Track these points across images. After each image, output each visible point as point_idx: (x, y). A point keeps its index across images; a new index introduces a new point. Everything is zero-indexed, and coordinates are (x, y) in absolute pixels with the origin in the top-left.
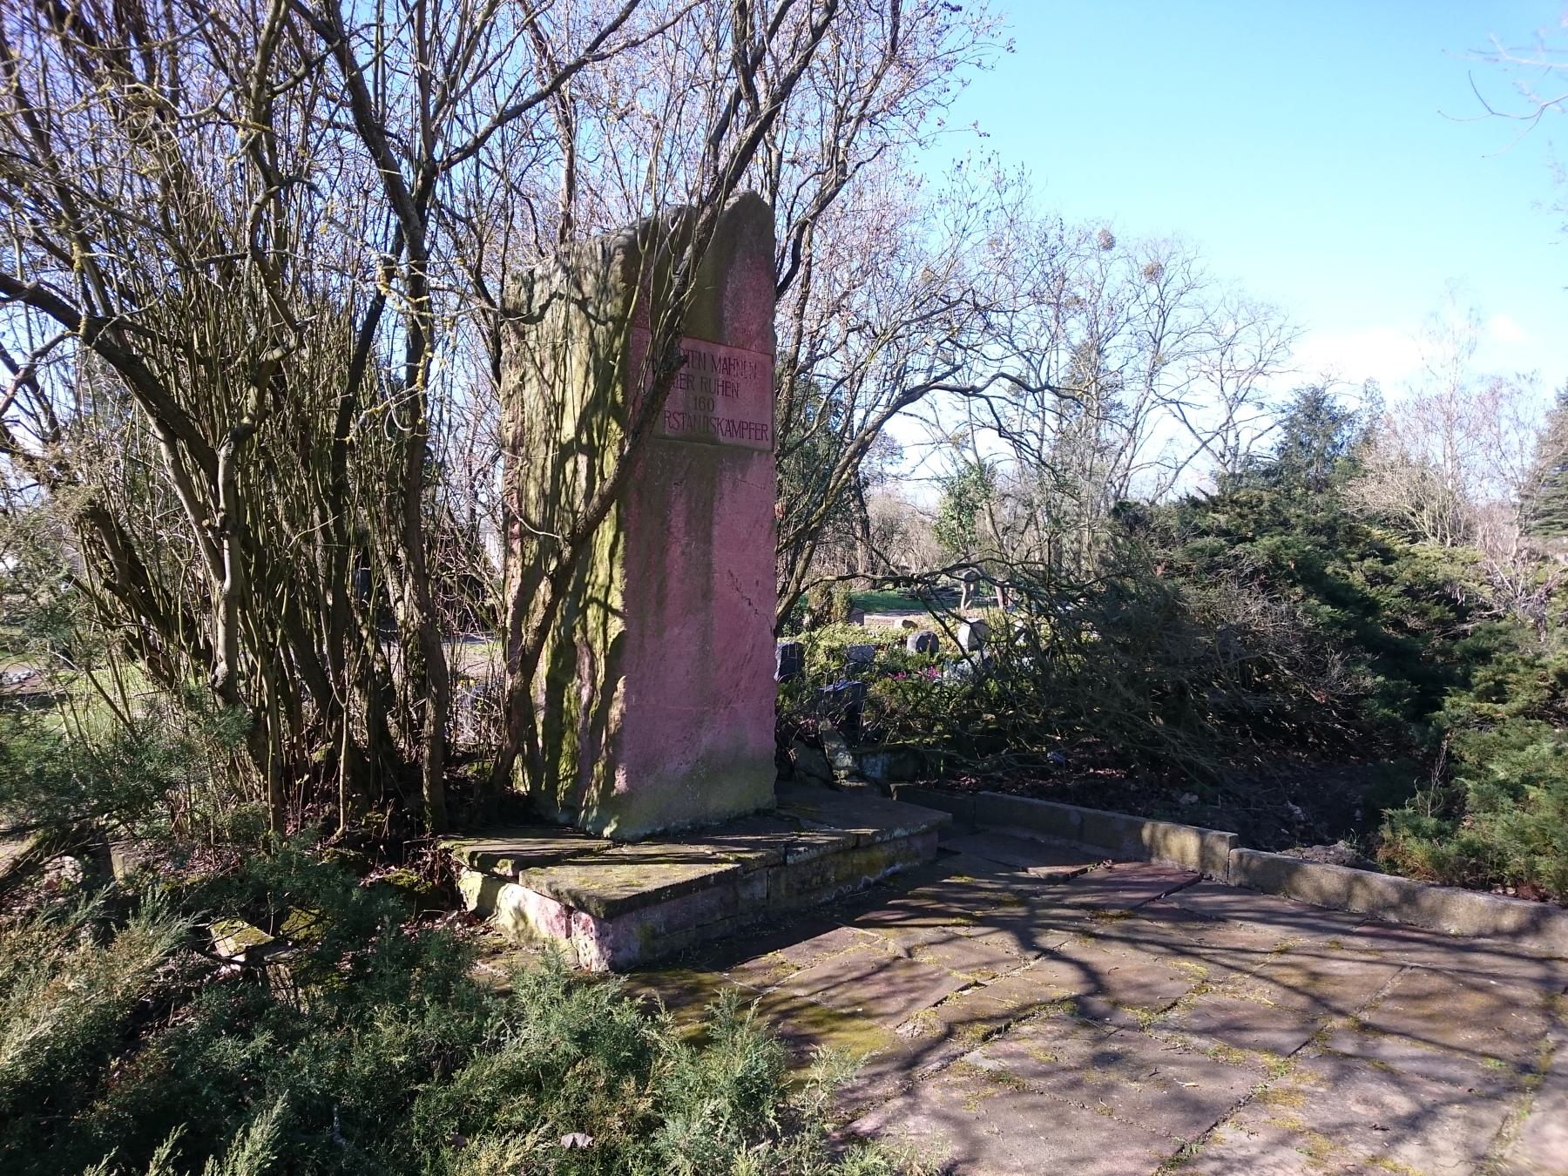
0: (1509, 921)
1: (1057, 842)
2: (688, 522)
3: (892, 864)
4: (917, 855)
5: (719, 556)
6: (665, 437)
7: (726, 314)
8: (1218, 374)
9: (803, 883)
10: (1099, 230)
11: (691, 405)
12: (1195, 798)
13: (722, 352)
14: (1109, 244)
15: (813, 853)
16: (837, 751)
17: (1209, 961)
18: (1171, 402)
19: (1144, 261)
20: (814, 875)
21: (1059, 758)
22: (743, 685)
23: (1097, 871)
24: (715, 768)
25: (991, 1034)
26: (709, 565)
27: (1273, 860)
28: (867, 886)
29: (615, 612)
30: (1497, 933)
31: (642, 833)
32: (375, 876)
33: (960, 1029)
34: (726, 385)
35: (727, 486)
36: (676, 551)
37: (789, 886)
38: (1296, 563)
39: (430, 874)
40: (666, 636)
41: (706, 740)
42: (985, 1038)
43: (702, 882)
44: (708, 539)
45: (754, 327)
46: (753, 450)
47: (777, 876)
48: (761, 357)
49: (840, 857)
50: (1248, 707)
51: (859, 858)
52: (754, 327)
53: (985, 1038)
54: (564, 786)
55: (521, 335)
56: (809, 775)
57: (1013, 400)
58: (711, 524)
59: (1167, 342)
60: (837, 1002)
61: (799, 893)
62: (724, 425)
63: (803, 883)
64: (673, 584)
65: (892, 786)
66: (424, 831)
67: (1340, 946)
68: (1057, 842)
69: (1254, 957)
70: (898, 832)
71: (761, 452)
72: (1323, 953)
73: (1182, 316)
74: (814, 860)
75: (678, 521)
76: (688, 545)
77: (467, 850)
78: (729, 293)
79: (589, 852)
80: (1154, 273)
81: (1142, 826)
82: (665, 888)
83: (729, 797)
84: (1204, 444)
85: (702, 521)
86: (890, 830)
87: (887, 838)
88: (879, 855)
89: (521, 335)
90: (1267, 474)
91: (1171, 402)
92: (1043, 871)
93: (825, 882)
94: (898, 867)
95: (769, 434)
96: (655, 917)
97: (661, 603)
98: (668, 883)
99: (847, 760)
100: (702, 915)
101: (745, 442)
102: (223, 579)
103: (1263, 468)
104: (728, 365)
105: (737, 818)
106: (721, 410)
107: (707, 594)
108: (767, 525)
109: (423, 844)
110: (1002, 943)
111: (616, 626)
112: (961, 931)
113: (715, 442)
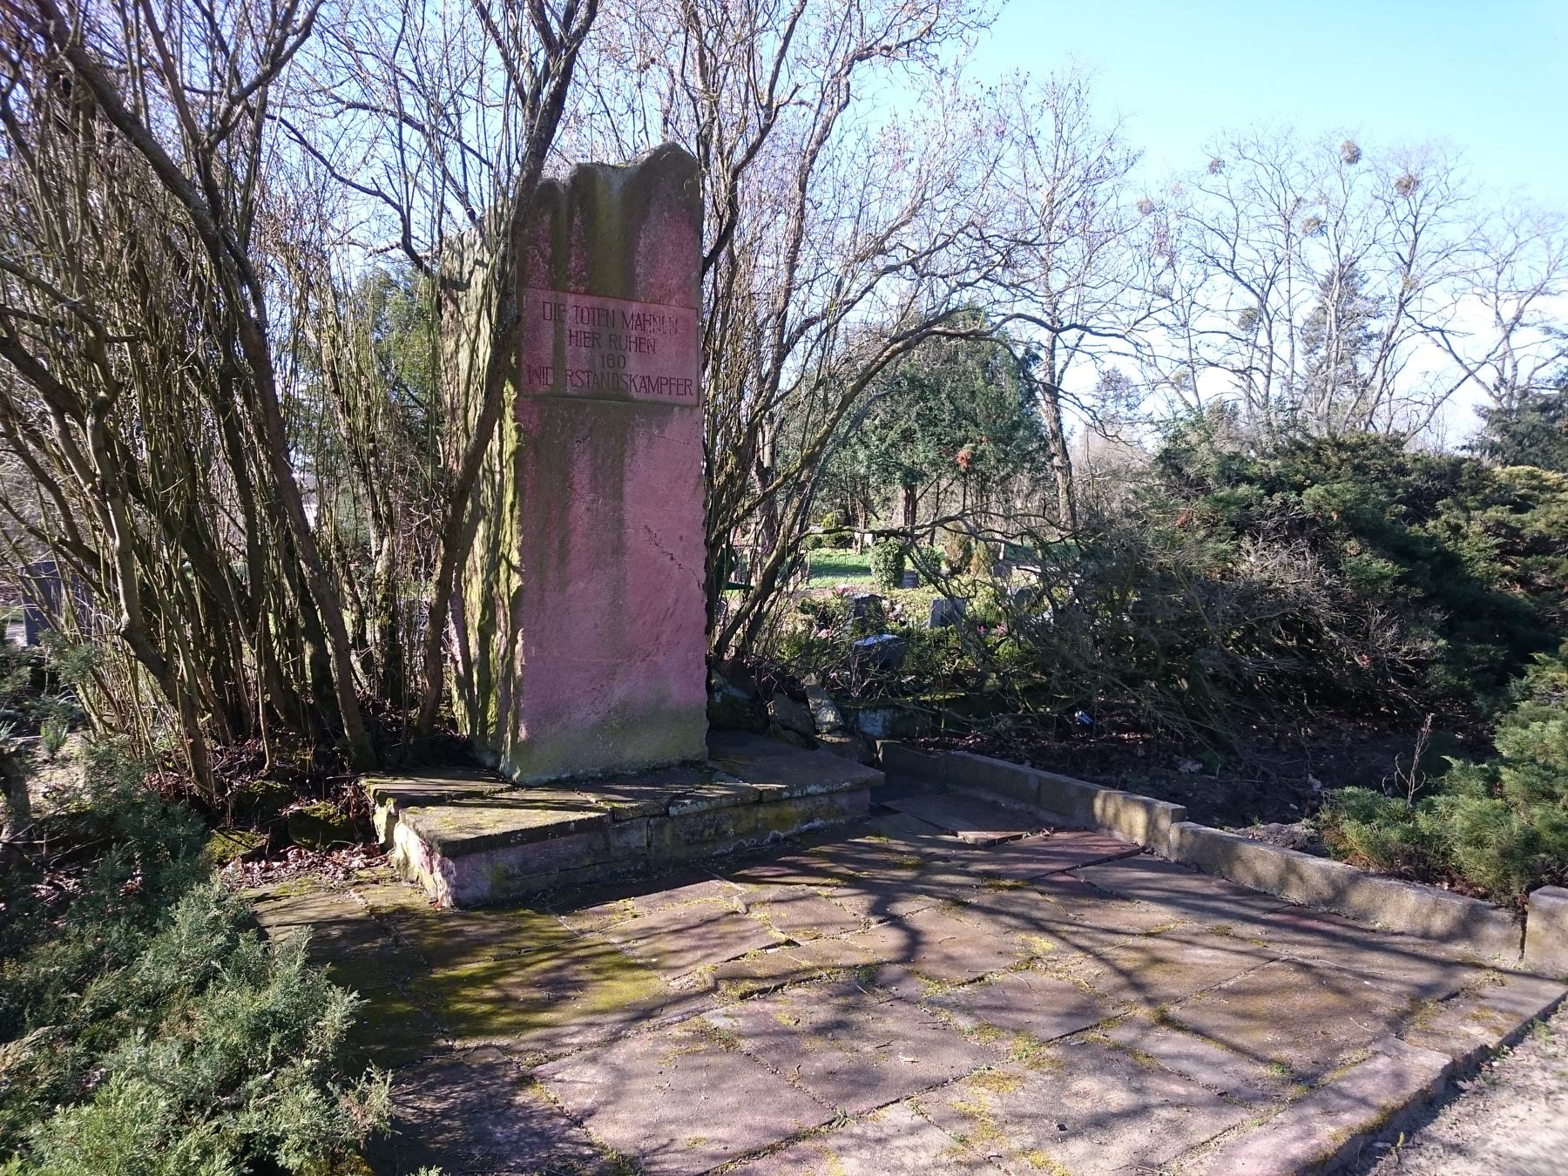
0: (1439, 923)
1: (1017, 807)
2: (594, 478)
3: (810, 820)
4: (842, 812)
5: (631, 512)
6: (568, 396)
7: (638, 270)
8: (1492, 297)
9: (693, 834)
10: (1342, 141)
11: (598, 362)
12: (1199, 766)
13: (635, 308)
14: (1354, 157)
15: (704, 805)
16: (819, 706)
17: (1063, 939)
18: (1433, 329)
19: (1398, 173)
20: (705, 827)
21: (1087, 720)
22: (664, 639)
23: (1030, 839)
24: (631, 719)
25: (752, 993)
26: (620, 522)
27: (1212, 836)
28: (776, 840)
29: (516, 569)
30: (1426, 935)
31: (545, 778)
32: (295, 807)
33: (723, 986)
34: (640, 342)
35: (641, 441)
36: (579, 508)
37: (675, 837)
38: (1338, 512)
39: (347, 808)
40: (570, 590)
41: (619, 692)
42: (743, 997)
43: (561, 828)
44: (619, 495)
45: (674, 282)
46: (674, 405)
47: (660, 827)
48: (683, 312)
49: (741, 810)
50: (1346, 667)
51: (762, 813)
52: (674, 282)
53: (743, 997)
54: (491, 730)
55: (455, 302)
56: (786, 728)
57: (1243, 335)
58: (622, 480)
59: (1423, 261)
60: (637, 953)
61: (688, 843)
62: (638, 381)
63: (693, 834)
64: (577, 540)
65: (878, 743)
66: (344, 769)
67: (1224, 933)
68: (1017, 807)
69: (1122, 939)
70: (811, 789)
71: (683, 407)
72: (1193, 939)
73: (1446, 229)
74: (706, 812)
75: (581, 477)
76: (593, 501)
77: (373, 787)
78: (642, 247)
79: (479, 794)
80: (1408, 186)
81: (1093, 795)
82: (514, 832)
83: (645, 748)
84: (1471, 374)
85: (610, 479)
86: (802, 786)
87: (797, 793)
88: (790, 810)
89: (455, 302)
90: (1544, 408)
91: (1433, 329)
92: (970, 836)
93: (721, 835)
94: (817, 823)
95: (694, 390)
96: (508, 859)
97: (563, 558)
98: (522, 827)
99: (830, 717)
100: (567, 860)
101: (665, 397)
102: (114, 537)
103: (1539, 401)
104: (642, 321)
105: (654, 769)
106: (634, 366)
107: (618, 549)
108: (692, 481)
109: (344, 781)
110: (853, 904)
111: (516, 581)
112: (825, 891)
113: (628, 399)
